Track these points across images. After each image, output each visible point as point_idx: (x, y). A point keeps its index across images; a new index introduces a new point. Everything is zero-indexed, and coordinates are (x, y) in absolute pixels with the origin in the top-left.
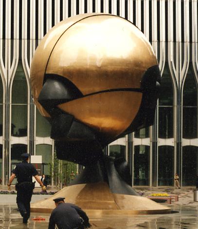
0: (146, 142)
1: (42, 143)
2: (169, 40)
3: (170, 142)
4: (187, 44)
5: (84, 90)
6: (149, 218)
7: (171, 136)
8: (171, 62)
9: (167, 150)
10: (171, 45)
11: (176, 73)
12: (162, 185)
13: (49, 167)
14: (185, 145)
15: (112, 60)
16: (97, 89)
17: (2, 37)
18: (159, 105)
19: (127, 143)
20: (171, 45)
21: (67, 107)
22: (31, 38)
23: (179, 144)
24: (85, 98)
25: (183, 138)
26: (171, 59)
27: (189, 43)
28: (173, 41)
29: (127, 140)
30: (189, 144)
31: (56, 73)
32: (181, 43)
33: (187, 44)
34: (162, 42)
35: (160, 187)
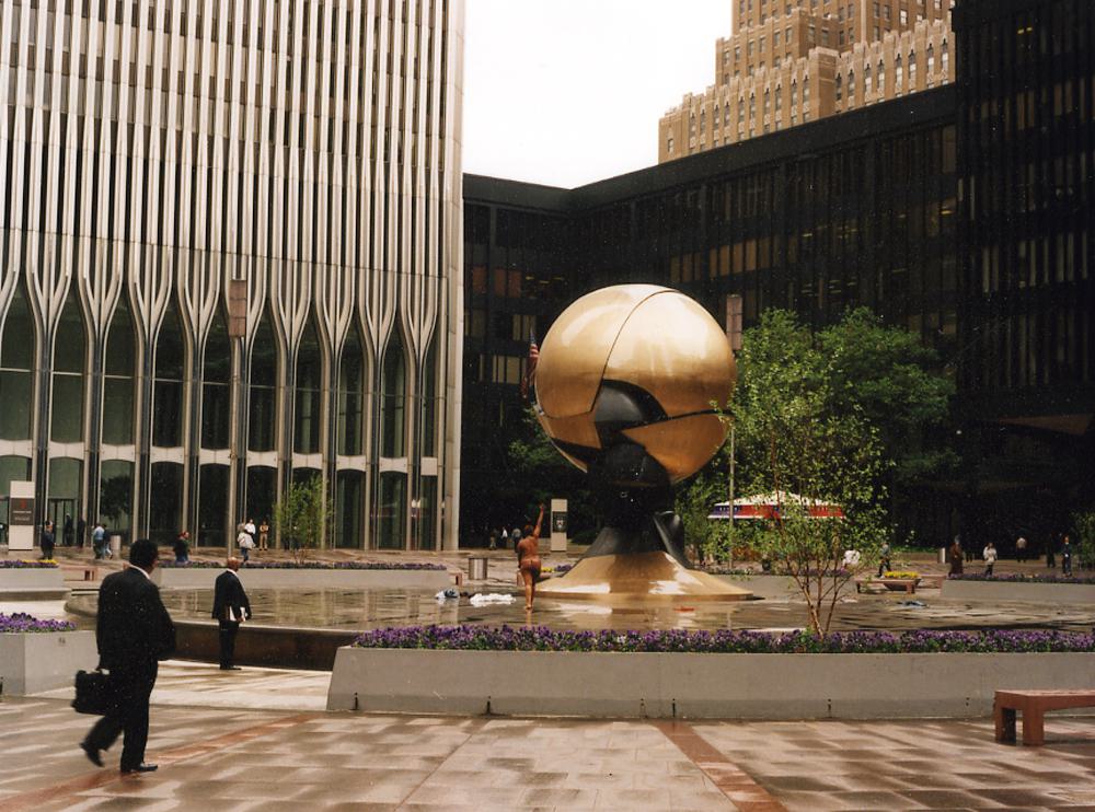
0: (127, 453)
1: (211, 461)
2: (115, 238)
3: (175, 455)
4: (168, 251)
5: (669, 408)
6: (730, 608)
7: (315, 449)
8: (84, 280)
9: (171, 469)
10: (136, 248)
11: (286, 321)
12: (209, 545)
13: (68, 504)
14: (254, 464)
15: (694, 365)
16: (688, 411)
17: (2, 224)
18: (106, 373)
19: (187, 459)
20: (136, 248)
21: (635, 434)
22: (98, 236)
23: (287, 463)
24: (669, 422)
25: (154, 444)
26: (183, 281)
27: (55, 236)
28: (20, 227)
29: (187, 452)
30: (304, 465)
31: (625, 380)
32: (155, 248)
33: (168, 251)
34: (84, 236)
35: (204, 549)
